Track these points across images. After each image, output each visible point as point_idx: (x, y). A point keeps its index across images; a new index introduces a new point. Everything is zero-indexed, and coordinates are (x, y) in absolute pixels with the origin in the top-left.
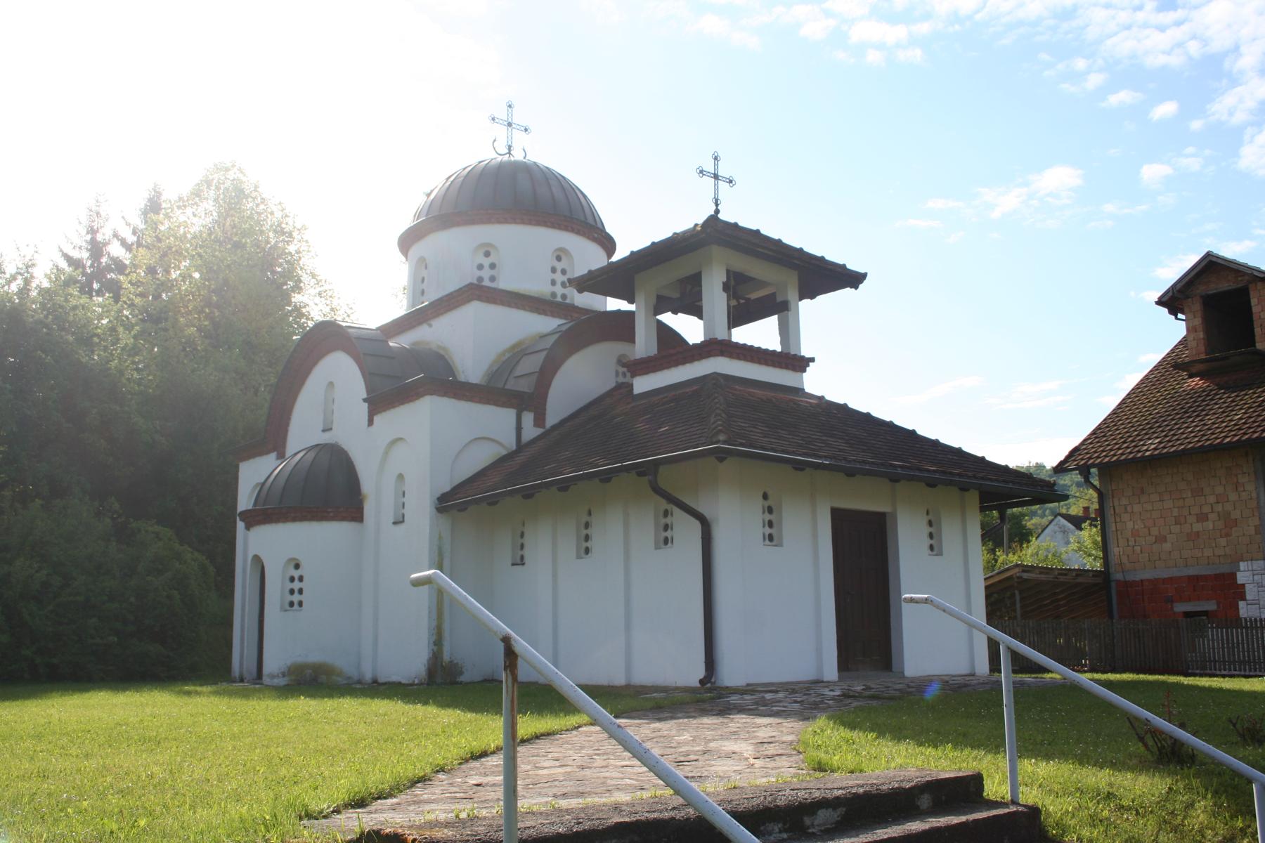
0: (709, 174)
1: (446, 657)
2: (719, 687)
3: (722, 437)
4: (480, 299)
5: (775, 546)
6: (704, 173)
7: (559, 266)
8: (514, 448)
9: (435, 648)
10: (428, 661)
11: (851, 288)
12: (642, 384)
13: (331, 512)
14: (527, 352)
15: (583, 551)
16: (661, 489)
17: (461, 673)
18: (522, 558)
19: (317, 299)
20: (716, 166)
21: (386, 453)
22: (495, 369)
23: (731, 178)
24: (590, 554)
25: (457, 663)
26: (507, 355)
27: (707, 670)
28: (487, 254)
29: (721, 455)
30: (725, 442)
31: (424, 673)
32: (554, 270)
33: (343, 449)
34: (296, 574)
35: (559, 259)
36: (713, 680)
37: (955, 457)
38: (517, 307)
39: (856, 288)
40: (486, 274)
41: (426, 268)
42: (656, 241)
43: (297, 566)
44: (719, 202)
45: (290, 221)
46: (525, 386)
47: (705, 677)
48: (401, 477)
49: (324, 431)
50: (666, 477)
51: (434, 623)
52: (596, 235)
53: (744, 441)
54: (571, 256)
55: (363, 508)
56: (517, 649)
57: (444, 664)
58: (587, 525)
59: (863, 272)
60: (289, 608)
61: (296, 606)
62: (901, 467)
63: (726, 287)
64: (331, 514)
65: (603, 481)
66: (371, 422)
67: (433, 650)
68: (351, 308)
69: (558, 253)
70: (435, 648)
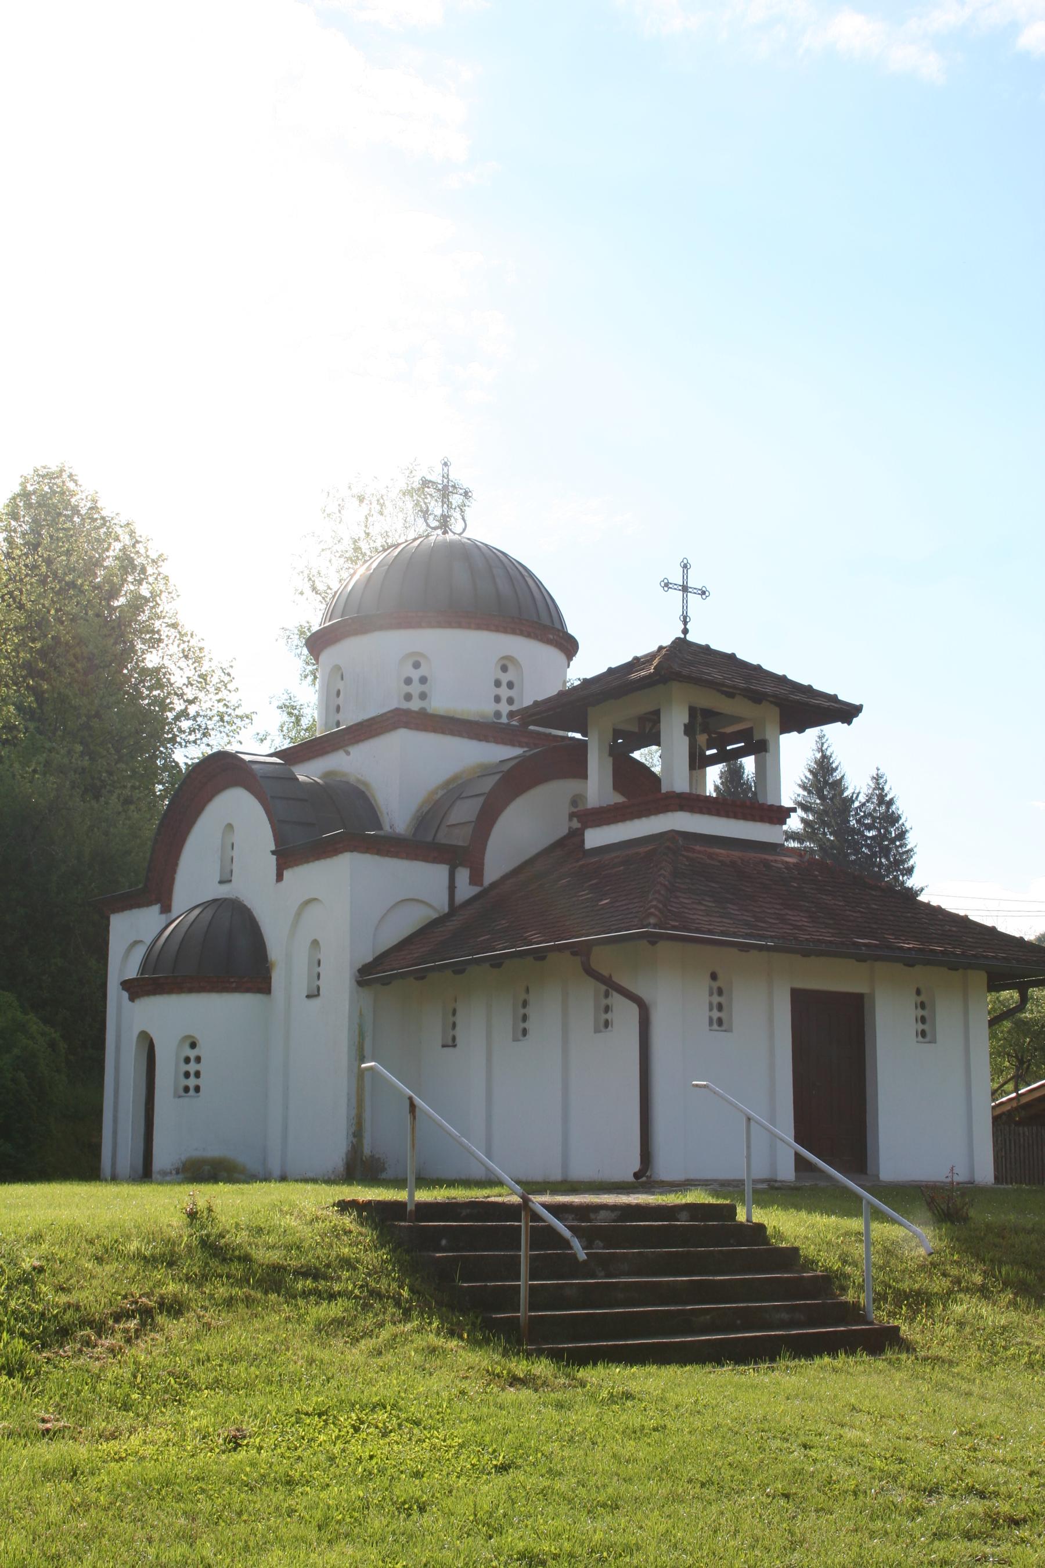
0: (676, 587)
1: (367, 1151)
2: (654, 1181)
3: (652, 920)
4: (407, 725)
5: (725, 1031)
6: (670, 586)
7: (505, 678)
8: (446, 910)
9: (355, 1140)
10: (347, 1154)
11: (843, 723)
12: (596, 838)
13: (232, 982)
14: (464, 795)
15: (520, 1033)
16: (593, 970)
17: (383, 1169)
18: (454, 1038)
19: (183, 663)
20: (685, 576)
21: (299, 914)
22: (425, 809)
23: (704, 589)
24: (527, 1037)
25: (379, 1158)
26: (440, 793)
27: (642, 1162)
28: (417, 665)
29: (653, 939)
30: (655, 926)
31: (342, 1169)
32: (498, 684)
33: (245, 906)
34: (192, 1054)
35: (504, 669)
36: (648, 1174)
37: (954, 929)
38: (452, 733)
39: (849, 723)
40: (415, 689)
41: (342, 679)
42: (613, 666)
43: (193, 1045)
44: (688, 620)
45: (140, 547)
46: (460, 838)
47: (640, 1171)
48: (315, 943)
49: (221, 882)
50: (603, 960)
51: (354, 1112)
52: (551, 637)
53: (677, 924)
54: (518, 663)
55: (270, 978)
56: (416, 1103)
57: (364, 1158)
58: (525, 1004)
59: (858, 703)
60: (184, 1094)
61: (192, 1092)
62: (865, 945)
63: (689, 730)
64: (234, 985)
65: (537, 959)
66: (280, 877)
67: (352, 1142)
68: (229, 675)
69: (505, 662)
70: (355, 1140)
